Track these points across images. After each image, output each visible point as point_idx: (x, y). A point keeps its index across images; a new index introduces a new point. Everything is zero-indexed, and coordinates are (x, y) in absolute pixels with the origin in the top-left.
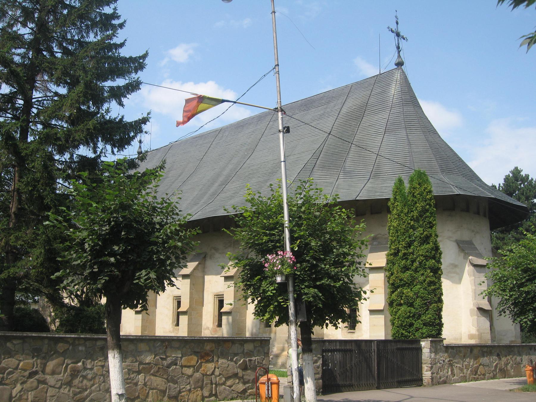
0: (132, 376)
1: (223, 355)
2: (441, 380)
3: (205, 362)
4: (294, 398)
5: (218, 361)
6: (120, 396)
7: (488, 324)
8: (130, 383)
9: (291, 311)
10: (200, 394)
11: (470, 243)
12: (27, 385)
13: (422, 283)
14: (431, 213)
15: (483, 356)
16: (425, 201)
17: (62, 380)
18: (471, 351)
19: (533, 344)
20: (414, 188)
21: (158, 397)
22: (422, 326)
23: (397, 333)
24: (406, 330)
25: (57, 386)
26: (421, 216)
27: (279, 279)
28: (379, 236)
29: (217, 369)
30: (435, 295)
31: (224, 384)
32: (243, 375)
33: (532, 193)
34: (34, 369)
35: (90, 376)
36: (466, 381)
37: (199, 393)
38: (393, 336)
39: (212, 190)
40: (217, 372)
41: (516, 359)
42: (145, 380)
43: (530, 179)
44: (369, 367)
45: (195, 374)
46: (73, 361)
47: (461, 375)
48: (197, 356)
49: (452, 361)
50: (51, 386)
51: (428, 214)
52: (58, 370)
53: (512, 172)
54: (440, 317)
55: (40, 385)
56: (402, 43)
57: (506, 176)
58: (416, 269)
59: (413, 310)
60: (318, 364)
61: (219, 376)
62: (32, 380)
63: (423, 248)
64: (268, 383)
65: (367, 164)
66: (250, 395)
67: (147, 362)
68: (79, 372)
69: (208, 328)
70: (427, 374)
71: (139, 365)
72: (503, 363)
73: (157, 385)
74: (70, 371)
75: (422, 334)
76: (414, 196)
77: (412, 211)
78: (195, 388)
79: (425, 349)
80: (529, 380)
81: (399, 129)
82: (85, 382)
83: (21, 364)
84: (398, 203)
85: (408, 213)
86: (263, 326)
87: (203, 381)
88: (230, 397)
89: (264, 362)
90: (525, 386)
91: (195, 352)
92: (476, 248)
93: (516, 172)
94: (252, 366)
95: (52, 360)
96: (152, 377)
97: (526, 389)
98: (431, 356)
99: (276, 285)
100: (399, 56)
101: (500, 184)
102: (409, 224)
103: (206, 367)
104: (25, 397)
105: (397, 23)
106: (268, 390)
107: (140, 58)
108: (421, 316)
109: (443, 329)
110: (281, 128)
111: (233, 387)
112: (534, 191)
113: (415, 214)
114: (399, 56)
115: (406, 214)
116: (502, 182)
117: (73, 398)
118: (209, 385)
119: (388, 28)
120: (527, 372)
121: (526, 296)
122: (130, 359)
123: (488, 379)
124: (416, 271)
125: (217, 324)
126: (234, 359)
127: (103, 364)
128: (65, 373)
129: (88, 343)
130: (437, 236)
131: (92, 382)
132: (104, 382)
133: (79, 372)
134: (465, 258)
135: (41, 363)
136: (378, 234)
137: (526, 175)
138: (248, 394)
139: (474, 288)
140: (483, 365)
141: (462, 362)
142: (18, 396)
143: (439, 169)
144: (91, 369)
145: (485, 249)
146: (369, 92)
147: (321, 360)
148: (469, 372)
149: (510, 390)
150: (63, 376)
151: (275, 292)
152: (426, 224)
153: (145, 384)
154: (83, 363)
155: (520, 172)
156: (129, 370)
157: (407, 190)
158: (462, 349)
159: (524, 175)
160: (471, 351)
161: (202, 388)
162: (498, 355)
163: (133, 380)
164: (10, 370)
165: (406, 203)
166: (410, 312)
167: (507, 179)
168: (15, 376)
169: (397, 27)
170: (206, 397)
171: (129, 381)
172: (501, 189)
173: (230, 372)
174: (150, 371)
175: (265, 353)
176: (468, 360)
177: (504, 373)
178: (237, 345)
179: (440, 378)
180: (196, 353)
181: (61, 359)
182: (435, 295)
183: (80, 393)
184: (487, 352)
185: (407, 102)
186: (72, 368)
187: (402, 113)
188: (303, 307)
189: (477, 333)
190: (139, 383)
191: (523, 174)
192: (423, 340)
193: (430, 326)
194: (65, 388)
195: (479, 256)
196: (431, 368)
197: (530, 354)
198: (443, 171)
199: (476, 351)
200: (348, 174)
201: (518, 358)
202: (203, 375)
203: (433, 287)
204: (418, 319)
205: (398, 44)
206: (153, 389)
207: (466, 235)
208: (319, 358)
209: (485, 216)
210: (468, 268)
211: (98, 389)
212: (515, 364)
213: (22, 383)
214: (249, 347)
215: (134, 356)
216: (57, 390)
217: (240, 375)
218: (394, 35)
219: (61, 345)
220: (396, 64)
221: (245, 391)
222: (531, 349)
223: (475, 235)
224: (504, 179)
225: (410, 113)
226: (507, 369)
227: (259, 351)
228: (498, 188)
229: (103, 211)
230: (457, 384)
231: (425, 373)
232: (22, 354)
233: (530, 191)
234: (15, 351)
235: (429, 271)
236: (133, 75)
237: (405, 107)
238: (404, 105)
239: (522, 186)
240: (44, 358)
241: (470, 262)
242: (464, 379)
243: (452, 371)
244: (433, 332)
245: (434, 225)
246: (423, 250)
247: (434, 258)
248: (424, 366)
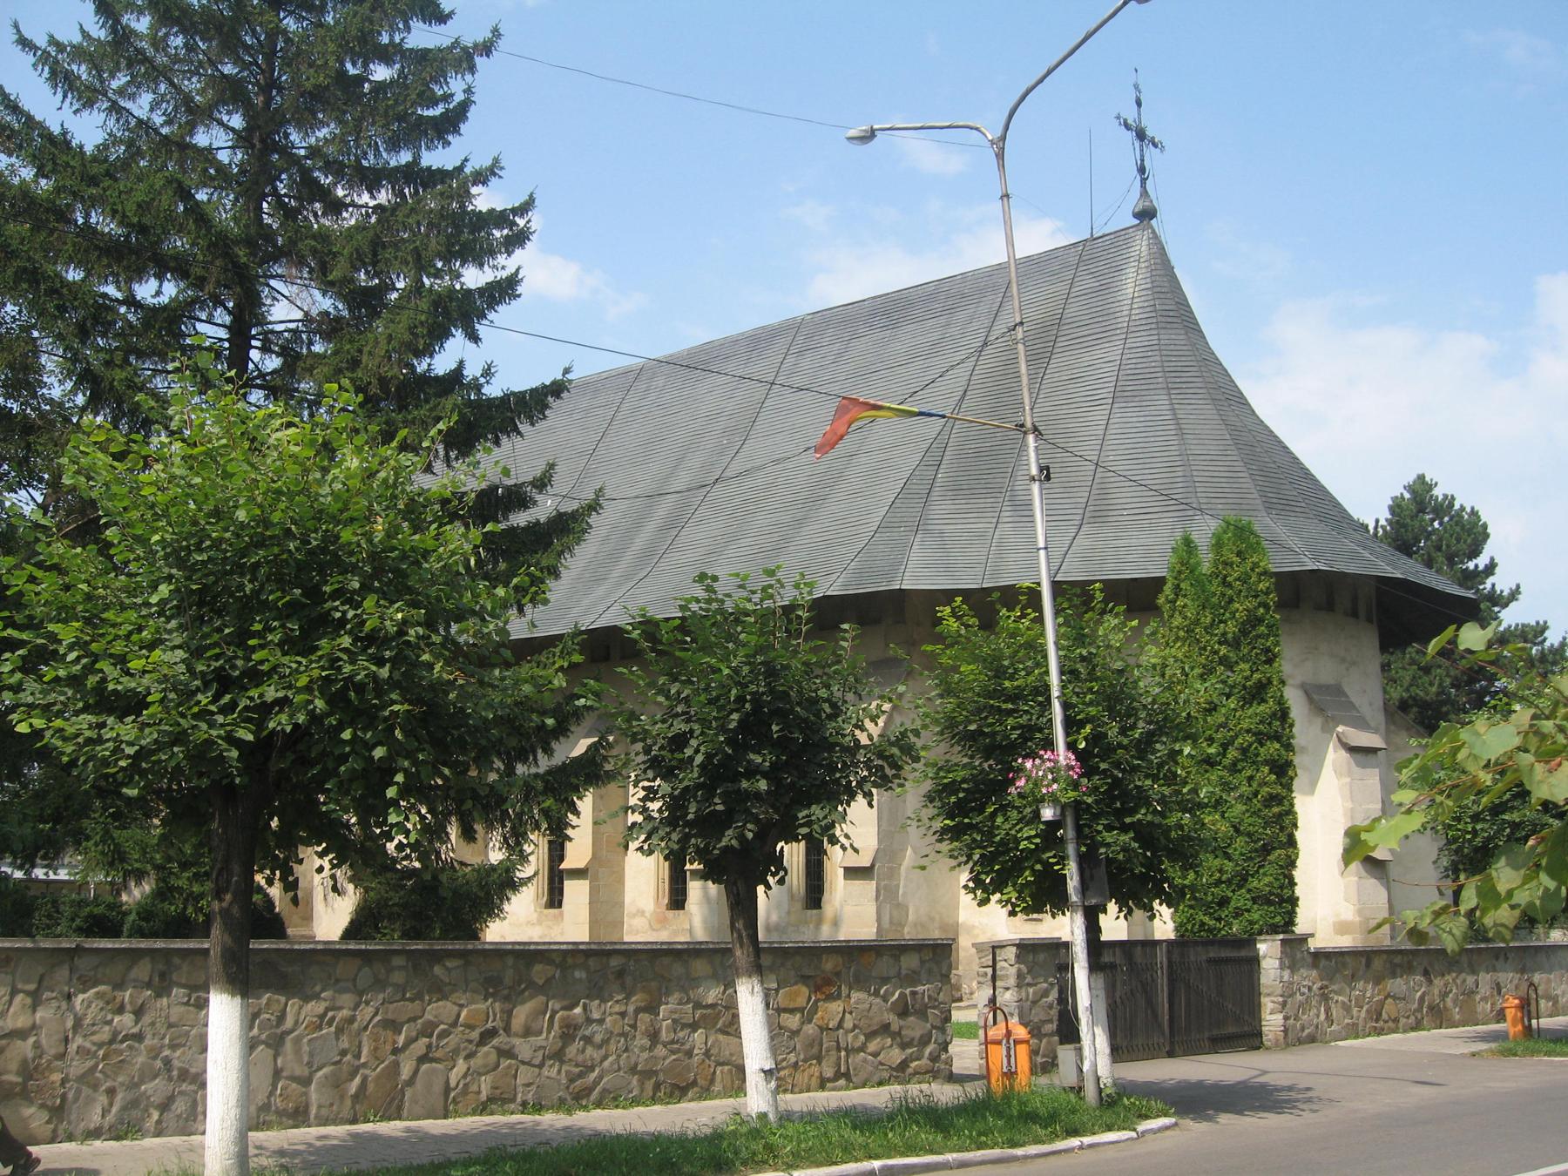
0: (681, 1034)
1: (860, 982)
2: (1305, 1034)
3: (824, 1000)
4: (1085, 1070)
5: (849, 996)
6: (768, 1073)
7: (1383, 894)
8: (678, 1051)
9: (1073, 884)
10: (817, 1074)
11: (1336, 691)
12: (477, 1062)
13: (1250, 800)
14: (1269, 627)
15: (1394, 975)
16: (1256, 597)
17: (545, 1048)
18: (1368, 965)
20: (1225, 563)
21: (733, 1082)
22: (1249, 903)
23: (1189, 921)
24: (1211, 914)
25: (537, 1061)
26: (1244, 633)
27: (1048, 813)
29: (847, 1016)
30: (1282, 829)
31: (862, 1049)
32: (901, 1028)
33: (1462, 546)
34: (490, 1025)
35: (598, 1038)
36: (1357, 1037)
37: (815, 1070)
38: (1176, 930)
39: (641, 540)
40: (848, 1024)
41: (1464, 981)
42: (706, 1043)
43: (1457, 506)
44: (1151, 1003)
45: (805, 1028)
46: (565, 1003)
47: (1346, 1021)
48: (807, 986)
49: (1327, 987)
50: (523, 1063)
51: (1262, 629)
52: (535, 1026)
53: (1409, 488)
54: (1292, 884)
55: (502, 1060)
56: (1152, 157)
57: (1394, 499)
58: (1234, 764)
59: (1229, 866)
60: (1050, 999)
61: (853, 1030)
62: (486, 1049)
63: (1250, 712)
64: (1008, 1042)
66: (916, 1073)
67: (710, 1002)
68: (577, 1027)
69: (642, 913)
70: (1272, 1021)
71: (694, 1008)
72: (1436, 992)
73: (731, 1055)
74: (561, 1028)
75: (1251, 923)
76: (1224, 583)
77: (1221, 622)
78: (805, 1061)
79: (1268, 959)
80: (1512, 1031)
81: (1152, 392)
82: (589, 1050)
83: (463, 1015)
84: (1189, 603)
85: (1212, 625)
86: (799, 905)
87: (821, 1045)
88: (876, 1078)
89: (941, 997)
90: (1506, 1045)
91: (802, 976)
92: (1351, 703)
93: (1421, 489)
94: (917, 1006)
95: (523, 1002)
96: (721, 1037)
97: (1510, 1050)
98: (1282, 977)
99: (1042, 827)
100: (1144, 193)
101: (1377, 521)
102: (1216, 652)
103: (825, 1011)
104: (474, 1088)
105: (1139, 103)
106: (1009, 1056)
107: (515, 211)
108: (1246, 880)
109: (1298, 910)
110: (1034, 471)
111: (882, 1055)
112: (1469, 541)
113: (1231, 628)
114: (1144, 193)
115: (1208, 629)
116: (1384, 515)
117: (568, 1088)
118: (834, 1052)
119: (1118, 117)
120: (1508, 1011)
121: (1512, 833)
122: (676, 996)
123: (1405, 1031)
124: (1234, 769)
125: (666, 901)
126: (882, 992)
127: (623, 1008)
128: (549, 1032)
129: (592, 962)
130: (1283, 682)
131: (603, 1051)
132: (626, 1050)
133: (577, 1027)
134: (1328, 728)
135: (502, 1011)
137: (1446, 496)
138: (910, 1070)
139: (1349, 805)
140: (1395, 998)
141: (1348, 990)
142: (461, 1086)
143: (1259, 502)
144: (601, 1021)
145: (1371, 704)
147: (1056, 989)
148: (1363, 1014)
149: (1473, 1055)
150: (548, 1039)
151: (1038, 840)
152: (1257, 654)
153: (707, 1054)
154: (585, 1008)
155: (1430, 487)
156: (674, 1021)
157: (1206, 568)
158: (1348, 959)
159: (1440, 498)
160: (1368, 965)
161: (819, 1059)
162: (1426, 973)
163: (683, 1044)
164: (442, 1027)
165: (1207, 600)
166: (1220, 871)
167: (1396, 507)
168: (452, 1040)
169: (1139, 114)
170: (829, 1080)
171: (675, 1046)
172: (1380, 531)
173: (876, 1020)
174: (716, 1023)
175: (942, 975)
176: (1360, 985)
177: (1439, 1017)
178: (885, 958)
179: (1303, 1029)
180: (805, 979)
181: (542, 998)
182: (1282, 829)
183: (581, 1075)
184: (1400, 966)
185: (1170, 320)
186: (563, 1019)
187: (1156, 347)
188: (1101, 872)
189: (1358, 919)
190: (696, 1052)
191: (1438, 492)
192: (1262, 937)
193: (1270, 903)
194: (551, 1066)
195: (1361, 723)
196: (1284, 1004)
197: (1495, 970)
198: (1269, 506)
199: (1377, 963)
201: (1470, 980)
202: (820, 1028)
203: (1276, 810)
204: (1240, 887)
205: (1142, 160)
206: (722, 1064)
207: (1325, 670)
208: (1052, 985)
209: (1369, 620)
210: (1334, 757)
211: (616, 1066)
212: (1463, 994)
213: (468, 1057)
214: (910, 962)
215: (683, 989)
216: (537, 1070)
217: (895, 1027)
218: (1130, 136)
219: (538, 967)
220: (1136, 215)
221: (904, 1065)
222: (1497, 958)
223: (1347, 669)
226: (1445, 1007)
227: (930, 971)
228: (1372, 531)
230: (1340, 1043)
231: (1268, 1017)
232: (465, 992)
233: (1458, 541)
234: (450, 984)
235: (1266, 769)
236: (501, 259)
237: (1162, 331)
238: (1160, 325)
239: (1436, 524)
240: (507, 998)
241: (1340, 740)
242: (1354, 1032)
243: (1328, 1011)
244: (1278, 919)
245: (1275, 656)
246: (1250, 717)
247: (1277, 737)
248: (1264, 1000)
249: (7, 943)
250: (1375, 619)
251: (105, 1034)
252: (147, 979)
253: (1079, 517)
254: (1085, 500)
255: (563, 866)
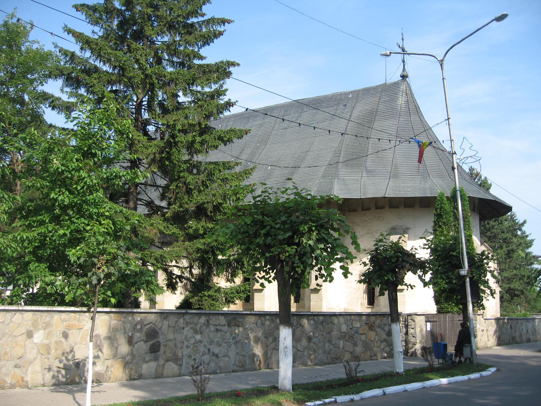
19: (503, 388)
100: (404, 69)
105: (403, 40)
114: (404, 69)
129: (315, 318)
146: (377, 99)
155: (473, 169)
200: (370, 173)
205: (404, 58)
220: (401, 76)
224: (83, 34)
249: (2, 308)
250: (476, 211)
251: (193, 341)
252: (203, 323)
253: (389, 176)
254: (390, 170)
255: (254, 288)
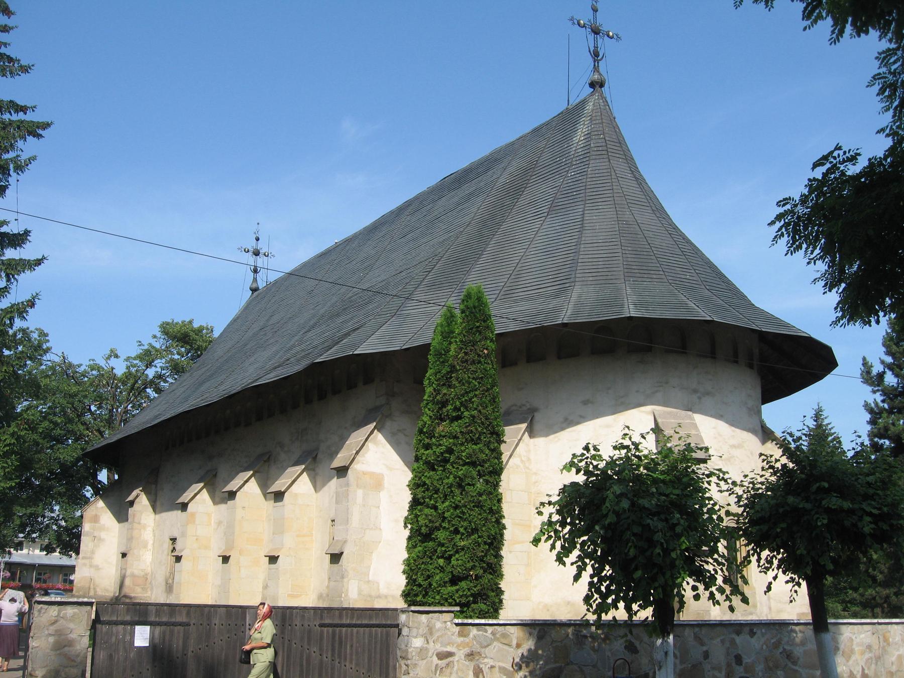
28: (514, 408)
56: (606, 46)
65: (501, 274)
100: (596, 69)
136: (513, 406)
169: (595, 18)
223: (700, 398)
225: (601, 171)
229: (120, 392)
